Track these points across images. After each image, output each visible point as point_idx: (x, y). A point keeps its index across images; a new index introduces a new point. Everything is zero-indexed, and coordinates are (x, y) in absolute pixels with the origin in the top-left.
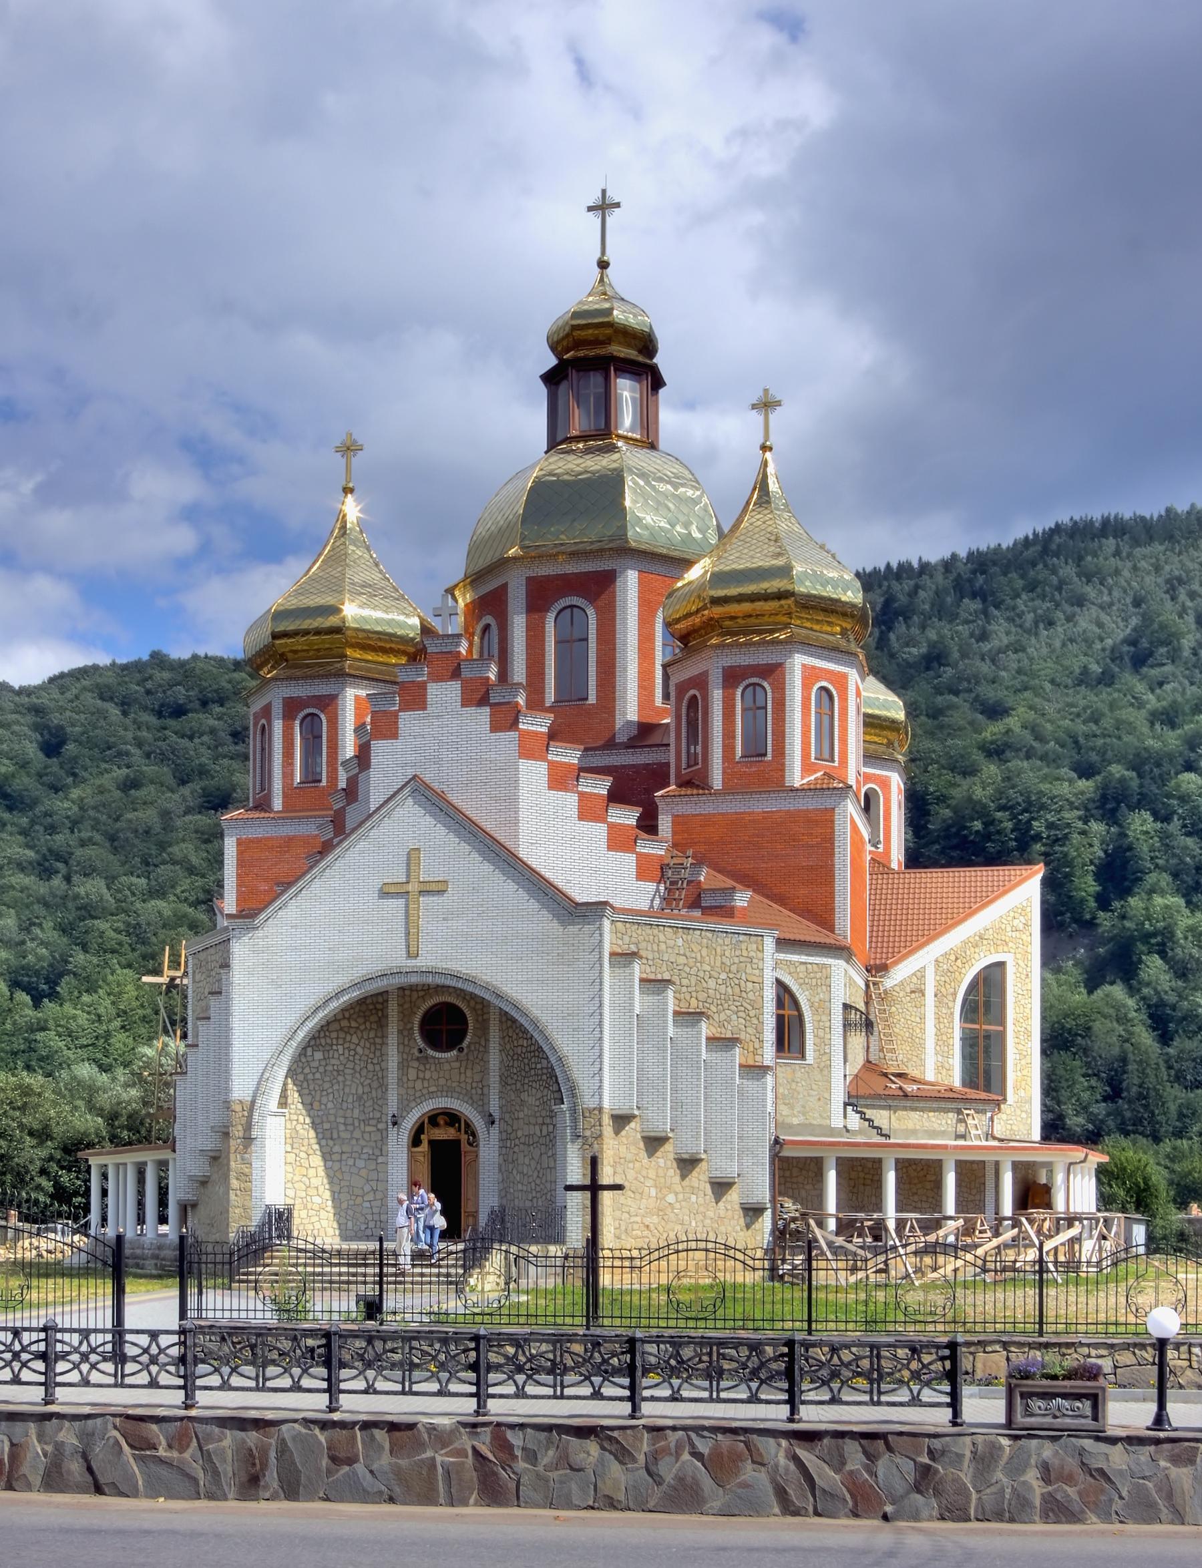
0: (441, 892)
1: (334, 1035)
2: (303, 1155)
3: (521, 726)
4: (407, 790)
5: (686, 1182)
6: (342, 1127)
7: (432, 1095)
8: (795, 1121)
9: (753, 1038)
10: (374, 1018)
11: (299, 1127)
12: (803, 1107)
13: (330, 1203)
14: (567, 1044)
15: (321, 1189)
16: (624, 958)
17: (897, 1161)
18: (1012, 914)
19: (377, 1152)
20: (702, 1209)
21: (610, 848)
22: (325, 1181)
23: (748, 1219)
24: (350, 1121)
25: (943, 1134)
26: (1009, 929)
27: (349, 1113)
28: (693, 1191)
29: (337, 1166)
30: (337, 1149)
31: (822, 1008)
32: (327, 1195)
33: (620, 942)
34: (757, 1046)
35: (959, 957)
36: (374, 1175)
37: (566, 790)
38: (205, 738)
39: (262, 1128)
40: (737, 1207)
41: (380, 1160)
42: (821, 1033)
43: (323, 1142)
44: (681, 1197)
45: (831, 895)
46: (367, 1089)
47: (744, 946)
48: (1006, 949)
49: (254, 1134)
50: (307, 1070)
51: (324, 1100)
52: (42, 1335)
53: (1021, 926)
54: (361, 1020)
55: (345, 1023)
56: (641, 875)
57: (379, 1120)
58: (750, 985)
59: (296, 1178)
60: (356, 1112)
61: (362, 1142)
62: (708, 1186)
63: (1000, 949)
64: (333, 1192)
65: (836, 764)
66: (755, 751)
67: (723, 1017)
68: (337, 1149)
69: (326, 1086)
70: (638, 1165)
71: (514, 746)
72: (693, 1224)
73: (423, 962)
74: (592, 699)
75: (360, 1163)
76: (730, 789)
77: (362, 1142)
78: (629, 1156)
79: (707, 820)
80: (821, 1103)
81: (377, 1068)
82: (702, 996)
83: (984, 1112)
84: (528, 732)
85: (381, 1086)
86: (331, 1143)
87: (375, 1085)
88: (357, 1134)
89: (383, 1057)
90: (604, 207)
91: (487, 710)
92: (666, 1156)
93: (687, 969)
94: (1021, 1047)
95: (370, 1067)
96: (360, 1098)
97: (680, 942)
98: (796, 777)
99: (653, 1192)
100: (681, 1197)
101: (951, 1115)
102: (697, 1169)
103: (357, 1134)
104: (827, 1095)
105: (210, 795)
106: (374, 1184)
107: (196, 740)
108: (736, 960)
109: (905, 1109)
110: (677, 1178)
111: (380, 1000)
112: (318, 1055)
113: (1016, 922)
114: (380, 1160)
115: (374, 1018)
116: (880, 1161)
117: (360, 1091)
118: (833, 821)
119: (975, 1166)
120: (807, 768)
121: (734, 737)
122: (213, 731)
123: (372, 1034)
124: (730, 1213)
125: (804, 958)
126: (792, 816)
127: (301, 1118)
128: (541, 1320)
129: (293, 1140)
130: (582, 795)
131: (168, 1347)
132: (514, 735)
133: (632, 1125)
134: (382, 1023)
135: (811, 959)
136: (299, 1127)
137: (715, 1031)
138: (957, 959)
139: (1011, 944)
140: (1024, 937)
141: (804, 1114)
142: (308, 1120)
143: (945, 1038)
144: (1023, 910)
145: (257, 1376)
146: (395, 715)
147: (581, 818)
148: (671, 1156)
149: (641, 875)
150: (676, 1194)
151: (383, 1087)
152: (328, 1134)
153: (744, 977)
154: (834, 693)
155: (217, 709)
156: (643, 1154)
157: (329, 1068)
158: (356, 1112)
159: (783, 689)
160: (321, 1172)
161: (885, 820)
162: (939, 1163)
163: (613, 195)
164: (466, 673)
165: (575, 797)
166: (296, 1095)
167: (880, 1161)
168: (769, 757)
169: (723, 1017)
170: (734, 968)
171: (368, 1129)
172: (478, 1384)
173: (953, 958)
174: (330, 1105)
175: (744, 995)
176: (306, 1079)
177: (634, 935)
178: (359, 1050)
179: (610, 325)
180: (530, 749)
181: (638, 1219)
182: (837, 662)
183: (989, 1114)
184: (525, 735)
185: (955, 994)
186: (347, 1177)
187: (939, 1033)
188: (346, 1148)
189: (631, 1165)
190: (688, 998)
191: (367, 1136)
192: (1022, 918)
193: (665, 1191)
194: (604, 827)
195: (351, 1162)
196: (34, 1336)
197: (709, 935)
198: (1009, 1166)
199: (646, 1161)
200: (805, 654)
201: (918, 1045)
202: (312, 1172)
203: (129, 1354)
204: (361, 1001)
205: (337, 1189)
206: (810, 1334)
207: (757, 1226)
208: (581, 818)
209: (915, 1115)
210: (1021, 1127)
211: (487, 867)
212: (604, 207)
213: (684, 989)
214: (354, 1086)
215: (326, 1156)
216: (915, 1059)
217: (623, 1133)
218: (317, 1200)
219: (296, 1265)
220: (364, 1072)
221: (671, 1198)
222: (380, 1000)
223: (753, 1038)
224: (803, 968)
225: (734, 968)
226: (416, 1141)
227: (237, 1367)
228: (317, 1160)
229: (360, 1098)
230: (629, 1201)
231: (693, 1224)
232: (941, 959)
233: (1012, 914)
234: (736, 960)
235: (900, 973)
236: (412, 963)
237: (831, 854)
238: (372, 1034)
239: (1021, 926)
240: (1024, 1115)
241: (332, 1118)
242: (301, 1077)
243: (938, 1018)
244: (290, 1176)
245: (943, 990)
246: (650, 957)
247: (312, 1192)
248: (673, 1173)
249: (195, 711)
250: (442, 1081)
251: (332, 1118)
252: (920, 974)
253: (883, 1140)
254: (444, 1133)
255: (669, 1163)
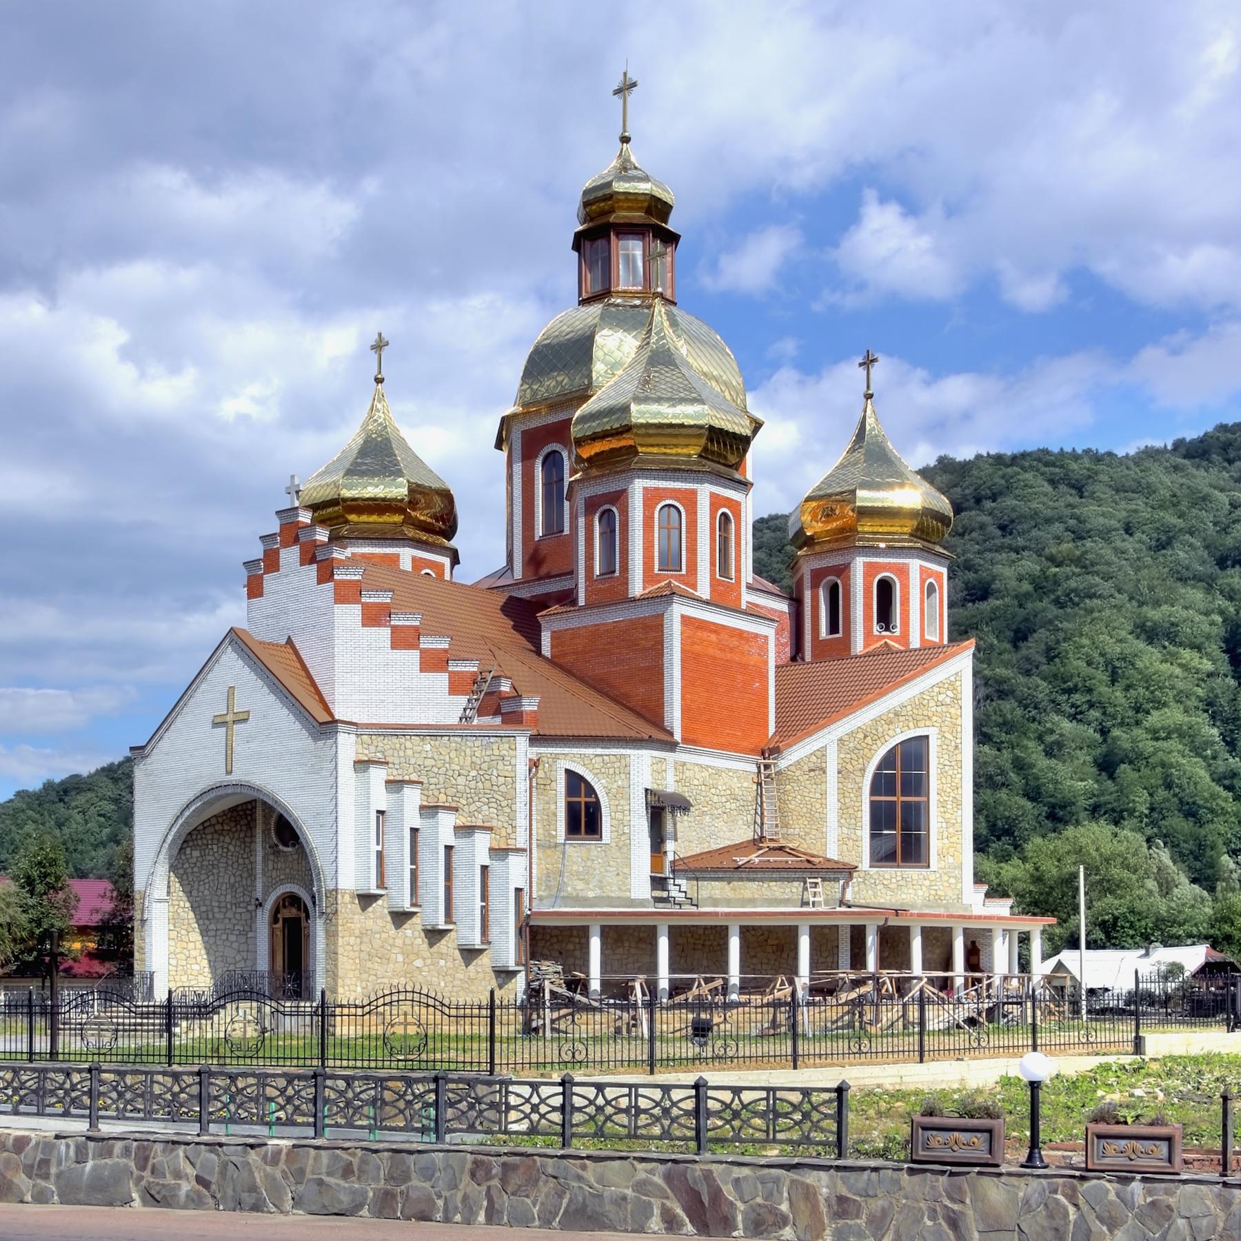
0: (245, 720)
1: (210, 837)
2: (183, 932)
3: (336, 577)
4: (227, 641)
5: (432, 950)
6: (216, 910)
7: (282, 882)
8: (591, 894)
9: (506, 825)
10: (244, 822)
11: (180, 910)
12: (600, 881)
13: (207, 970)
14: (313, 836)
15: (199, 958)
16: (362, 765)
17: (923, 929)
18: (936, 690)
19: (247, 929)
20: (450, 972)
21: (422, 670)
22: (203, 952)
23: (500, 980)
24: (223, 904)
25: (786, 902)
26: (932, 703)
27: (222, 898)
28: (442, 956)
29: (212, 940)
30: (212, 927)
31: (623, 794)
32: (205, 963)
33: (366, 752)
34: (509, 831)
35: (869, 735)
36: (243, 947)
37: (379, 625)
38: (974, 535)
39: (150, 912)
40: (489, 970)
41: (250, 935)
42: (619, 815)
43: (201, 922)
44: (429, 961)
45: (661, 692)
46: (238, 879)
47: (495, 747)
48: (928, 723)
49: (146, 917)
50: (186, 866)
51: (202, 888)
52: (560, 1089)
53: (948, 700)
54: (233, 824)
55: (218, 827)
56: (454, 689)
57: (249, 903)
58: (501, 780)
59: (178, 950)
60: (229, 897)
61: (234, 921)
62: (457, 952)
63: (921, 724)
64: (210, 961)
65: (684, 572)
66: (609, 571)
67: (473, 808)
68: (212, 927)
69: (203, 877)
70: (384, 935)
71: (331, 594)
72: (442, 984)
73: (233, 778)
74: (567, 531)
75: (232, 938)
76: (589, 606)
77: (234, 921)
78: (376, 928)
79: (574, 633)
80: (620, 878)
81: (247, 861)
82: (451, 791)
83: (836, 880)
84: (342, 581)
85: (250, 876)
86: (207, 922)
87: (245, 875)
88: (230, 915)
89: (252, 852)
90: (626, 88)
91: (315, 566)
92: (413, 931)
93: (435, 770)
94: (948, 816)
95: (241, 861)
96: (233, 886)
97: (428, 747)
98: (637, 587)
99: (400, 958)
100: (429, 961)
101: (796, 884)
102: (446, 938)
103: (230, 915)
104: (625, 870)
105: (974, 588)
106: (244, 954)
107: (966, 537)
108: (487, 759)
109: (741, 879)
110: (426, 946)
111: (249, 806)
112: (196, 853)
113: (941, 698)
114: (250, 935)
115: (244, 822)
116: (655, 927)
117: (232, 880)
118: (662, 625)
119: (826, 931)
120: (649, 577)
121: (593, 559)
122: (982, 527)
123: (242, 835)
124: (481, 975)
125: (599, 751)
126: (633, 624)
127: (182, 904)
128: (72, 1058)
129: (174, 920)
130: (394, 628)
131: (681, 1100)
132: (331, 584)
133: (380, 902)
134: (250, 826)
135: (606, 751)
136: (180, 910)
137: (462, 820)
138: (865, 737)
139: (934, 718)
140: (953, 711)
141: (601, 888)
142: (188, 905)
143: (851, 811)
144: (951, 685)
145: (768, 1127)
146: (261, 577)
147: (393, 648)
148: (420, 928)
149: (454, 689)
150: (424, 959)
151: (252, 875)
152: (204, 915)
153: (495, 773)
154: (682, 509)
155: (988, 504)
156: (390, 926)
157: (205, 863)
158: (229, 897)
159: (627, 512)
160: (200, 945)
161: (902, 605)
162: (906, 930)
163: (633, 76)
164: (302, 539)
165: (388, 630)
166: (178, 885)
167: (655, 927)
168: (617, 574)
169: (473, 808)
170: (485, 766)
171: (239, 910)
172: (315, 1116)
173: (861, 736)
174: (206, 892)
175: (495, 788)
176: (185, 873)
177: (380, 744)
178: (231, 847)
179: (610, 197)
180: (347, 594)
181: (386, 980)
182: (685, 480)
183: (841, 882)
184: (340, 585)
185: (863, 770)
186: (221, 949)
187: (844, 808)
188: (220, 926)
189: (377, 936)
190: (436, 793)
191: (238, 916)
192: (950, 693)
193: (412, 957)
194: (417, 653)
195: (224, 937)
196: (826, 1096)
197: (459, 739)
198: (919, 931)
199: (393, 931)
200: (643, 478)
201: (817, 819)
202: (191, 946)
203: (513, 1103)
204: (233, 810)
205: (213, 958)
206: (31, 1060)
207: (510, 986)
208: (393, 648)
209: (755, 885)
210: (950, 893)
211: (272, 697)
212: (626, 88)
213: (432, 787)
214: (227, 877)
215: (204, 932)
216: (814, 832)
217: (370, 909)
218: (196, 967)
219: (111, 1017)
220: (235, 866)
221: (419, 963)
222: (249, 806)
223: (506, 825)
224: (599, 759)
225: (485, 766)
226: (275, 920)
227: (749, 1119)
228: (196, 936)
229: (233, 886)
230: (376, 966)
231: (442, 984)
232: (846, 738)
233: (936, 690)
234: (487, 759)
235: (794, 755)
236: (229, 778)
237: (660, 654)
238: (242, 835)
239: (948, 700)
240: (952, 880)
241: (208, 903)
242: (181, 871)
243: (842, 793)
244: (172, 949)
245: (849, 766)
246: (397, 761)
247: (192, 961)
248: (421, 941)
249: (970, 509)
250: (288, 871)
251: (208, 903)
252: (822, 753)
253: (694, 909)
254: (290, 913)
255: (417, 934)
